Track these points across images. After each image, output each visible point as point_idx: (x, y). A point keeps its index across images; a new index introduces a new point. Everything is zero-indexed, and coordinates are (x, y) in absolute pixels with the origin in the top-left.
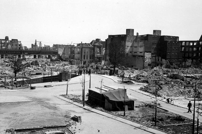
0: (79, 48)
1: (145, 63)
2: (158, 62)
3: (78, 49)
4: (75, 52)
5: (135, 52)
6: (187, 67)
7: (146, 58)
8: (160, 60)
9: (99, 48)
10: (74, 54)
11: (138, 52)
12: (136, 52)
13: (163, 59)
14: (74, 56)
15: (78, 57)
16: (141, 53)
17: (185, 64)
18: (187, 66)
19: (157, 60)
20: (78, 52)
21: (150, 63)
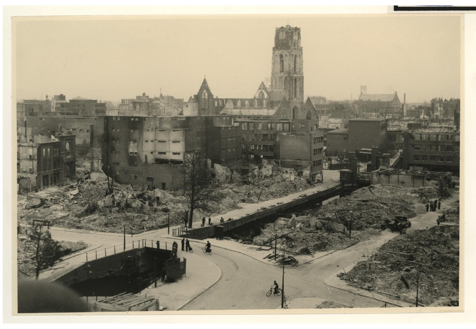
0: (32, 147)
6: (263, 178)
9: (70, 141)
12: (165, 153)
13: (215, 164)
15: (31, 168)
16: (159, 155)
17: (260, 173)
18: (263, 176)
20: (30, 156)
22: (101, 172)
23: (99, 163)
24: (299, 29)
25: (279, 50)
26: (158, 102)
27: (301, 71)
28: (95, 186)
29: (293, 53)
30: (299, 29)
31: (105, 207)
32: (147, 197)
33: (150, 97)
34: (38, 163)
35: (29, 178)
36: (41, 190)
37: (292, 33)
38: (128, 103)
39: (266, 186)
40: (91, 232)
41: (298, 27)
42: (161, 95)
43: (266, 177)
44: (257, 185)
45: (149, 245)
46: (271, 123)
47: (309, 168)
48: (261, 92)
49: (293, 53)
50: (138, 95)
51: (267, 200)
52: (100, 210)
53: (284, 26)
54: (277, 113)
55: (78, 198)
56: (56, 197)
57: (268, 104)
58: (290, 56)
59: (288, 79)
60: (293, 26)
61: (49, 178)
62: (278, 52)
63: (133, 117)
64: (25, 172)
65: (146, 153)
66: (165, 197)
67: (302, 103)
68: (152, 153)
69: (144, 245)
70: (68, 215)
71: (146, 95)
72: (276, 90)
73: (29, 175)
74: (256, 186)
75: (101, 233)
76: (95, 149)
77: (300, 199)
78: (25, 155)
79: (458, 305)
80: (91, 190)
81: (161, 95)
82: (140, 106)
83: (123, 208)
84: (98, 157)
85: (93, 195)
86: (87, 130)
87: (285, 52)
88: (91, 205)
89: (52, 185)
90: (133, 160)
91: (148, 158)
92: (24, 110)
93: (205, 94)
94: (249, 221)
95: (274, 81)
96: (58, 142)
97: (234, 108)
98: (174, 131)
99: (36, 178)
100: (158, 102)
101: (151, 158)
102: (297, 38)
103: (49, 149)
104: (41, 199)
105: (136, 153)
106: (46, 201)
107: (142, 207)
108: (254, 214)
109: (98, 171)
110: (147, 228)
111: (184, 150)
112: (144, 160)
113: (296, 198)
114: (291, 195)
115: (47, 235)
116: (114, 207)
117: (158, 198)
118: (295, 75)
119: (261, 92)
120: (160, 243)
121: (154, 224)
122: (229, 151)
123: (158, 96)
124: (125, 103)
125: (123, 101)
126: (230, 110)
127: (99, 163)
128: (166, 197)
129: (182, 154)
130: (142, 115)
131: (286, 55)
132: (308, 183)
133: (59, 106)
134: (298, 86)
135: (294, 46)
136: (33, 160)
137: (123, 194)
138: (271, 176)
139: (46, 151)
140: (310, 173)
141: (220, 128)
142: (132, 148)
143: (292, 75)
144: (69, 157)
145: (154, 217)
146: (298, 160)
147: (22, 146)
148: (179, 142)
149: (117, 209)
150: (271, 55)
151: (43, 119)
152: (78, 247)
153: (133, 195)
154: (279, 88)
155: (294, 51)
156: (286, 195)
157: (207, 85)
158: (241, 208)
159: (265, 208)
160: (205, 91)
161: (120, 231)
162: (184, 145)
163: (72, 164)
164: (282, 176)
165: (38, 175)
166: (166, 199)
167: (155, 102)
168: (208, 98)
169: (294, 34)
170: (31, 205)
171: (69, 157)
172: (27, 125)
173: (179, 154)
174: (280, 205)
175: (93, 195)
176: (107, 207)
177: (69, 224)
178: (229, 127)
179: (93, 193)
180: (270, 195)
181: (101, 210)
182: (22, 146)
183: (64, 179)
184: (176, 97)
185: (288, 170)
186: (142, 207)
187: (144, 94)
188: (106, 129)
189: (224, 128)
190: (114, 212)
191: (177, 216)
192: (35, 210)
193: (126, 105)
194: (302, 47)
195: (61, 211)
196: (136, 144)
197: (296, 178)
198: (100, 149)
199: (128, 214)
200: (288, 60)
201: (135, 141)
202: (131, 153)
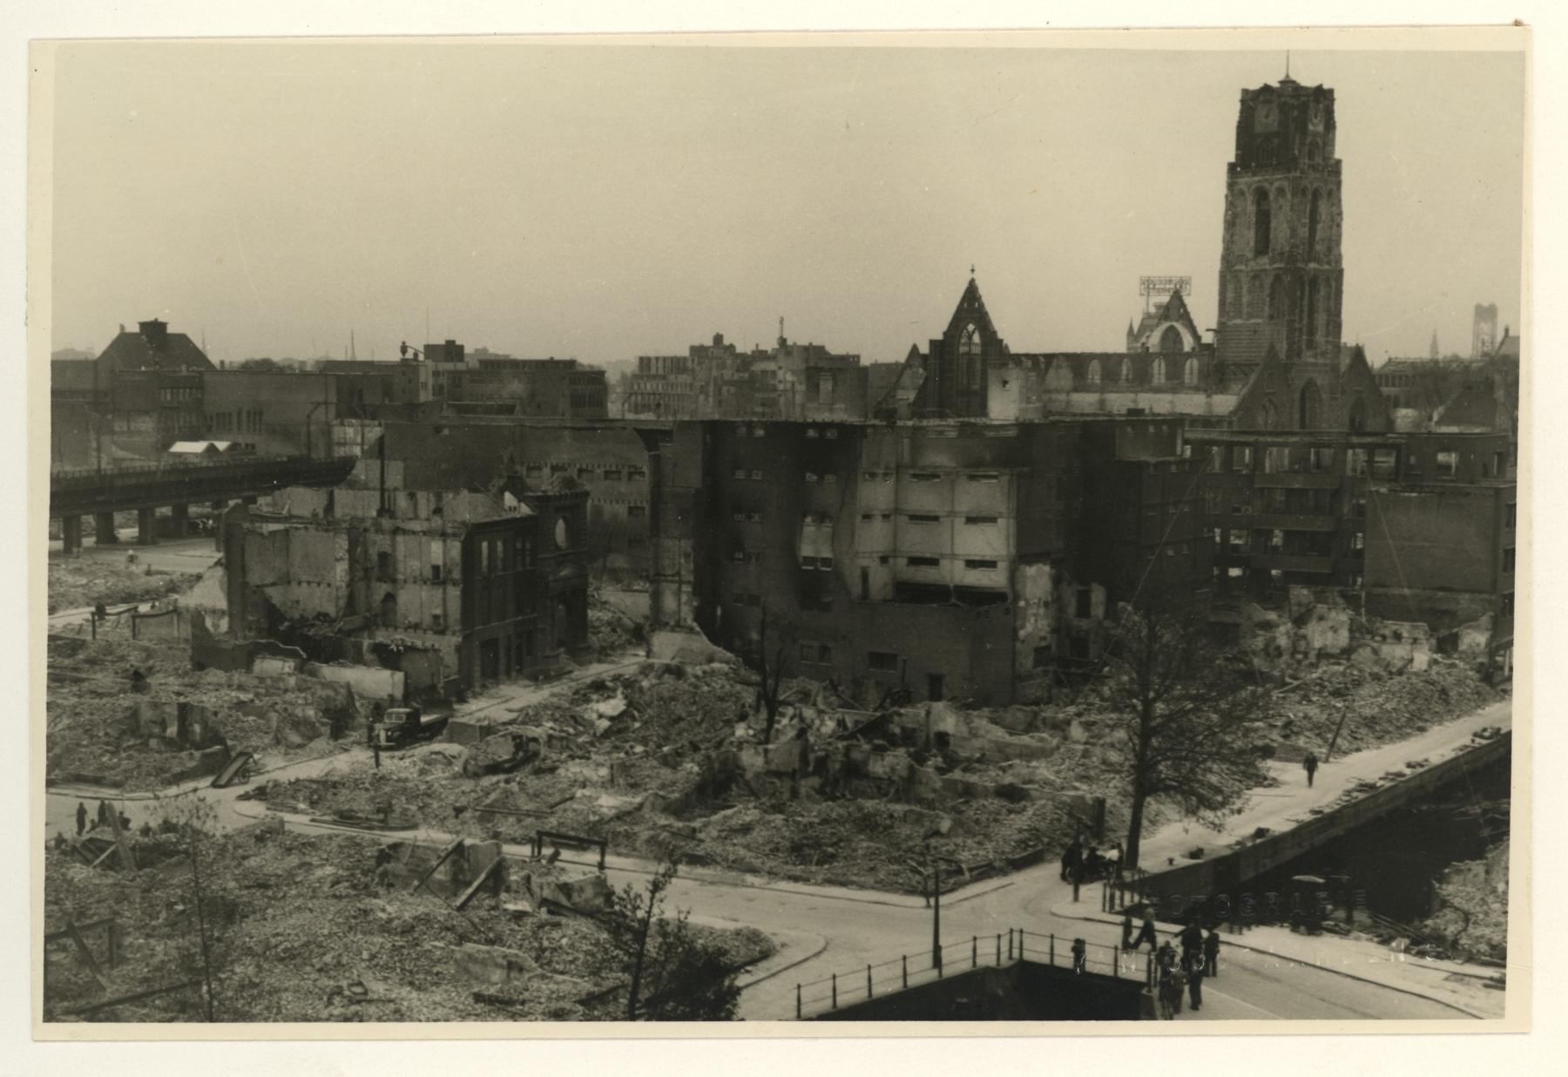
0: (443, 535)
1: (1018, 645)
2: (1084, 624)
3: (436, 547)
4: (401, 566)
5: (915, 561)
6: (1312, 659)
7: (1025, 609)
8: (1098, 611)
10: (394, 581)
11: (953, 556)
12: (933, 562)
14: (390, 598)
15: (438, 612)
16: (912, 569)
17: (1297, 638)
18: (1313, 654)
19: (1072, 609)
20: (436, 568)
21: (1043, 644)
22: (691, 630)
23: (684, 598)
24: (1331, 91)
25: (1254, 174)
26: (772, 366)
27: (1335, 252)
28: (683, 685)
29: (1305, 182)
30: (1331, 91)
31: (769, 773)
32: (897, 730)
33: (739, 350)
34: (466, 596)
35: (436, 651)
36: (475, 696)
37: (1304, 108)
38: (661, 372)
39: (1337, 693)
40: (749, 878)
41: (1326, 87)
42: (783, 341)
43: (1323, 655)
44: (1298, 687)
45: (1036, 952)
46: (1319, 446)
47: (1485, 620)
48: (1172, 328)
49: (1305, 182)
50: (697, 343)
51: (1358, 750)
52: (747, 783)
53: (1275, 84)
54: (1244, 407)
55: (626, 729)
56: (550, 724)
57: (1204, 374)
58: (1294, 195)
59: (1287, 279)
60: (1307, 80)
61: (502, 652)
62: (1247, 181)
63: (815, 425)
64: (416, 627)
65: (865, 562)
66: (973, 734)
67: (1335, 368)
68: (884, 560)
69: (1016, 953)
70: (640, 807)
71: (726, 342)
72: (1238, 321)
73: (430, 640)
74: (1294, 690)
75: (791, 886)
76: (668, 543)
77: (1482, 747)
78: (415, 564)
79: (1502, 1016)
80: (673, 699)
81: (783, 341)
82: (835, 384)
83: (837, 781)
84: (678, 574)
85: (680, 719)
86: (607, 473)
87: (1276, 181)
88: (716, 765)
89: (508, 674)
90: (814, 585)
91: (871, 581)
92: (333, 398)
93: (970, 337)
94: (1320, 839)
95: (1230, 287)
96: (529, 518)
97: (1076, 390)
98: (972, 477)
99: (459, 649)
100: (772, 366)
101: (880, 578)
102: (1321, 128)
103: (499, 544)
104: (514, 738)
105: (826, 561)
106: (532, 746)
107: (912, 778)
108: (1339, 811)
109: (679, 626)
110: (971, 870)
111: (1013, 550)
112: (857, 590)
113: (1467, 740)
114: (1436, 728)
115: (596, 895)
116: (806, 775)
117: (942, 738)
118: (1312, 265)
119: (1172, 328)
120: (1088, 948)
121: (988, 852)
122: (1170, 553)
123: (770, 345)
124: (653, 372)
125: (644, 362)
126: (1063, 397)
127: (684, 598)
128: (976, 736)
129: (1002, 566)
130: (841, 415)
131: (1281, 191)
132: (1482, 680)
133: (443, 380)
134: (1321, 306)
135: (1311, 155)
136: (444, 583)
137: (802, 719)
138: (1347, 652)
139: (492, 549)
140: (1488, 644)
141: (1141, 466)
142: (813, 543)
143: (1299, 265)
144: (565, 572)
145: (977, 822)
146: (1442, 589)
147: (405, 532)
148: (993, 520)
149: (815, 781)
150: (1223, 190)
151: (446, 432)
152: (743, 951)
153: (841, 723)
154: (1250, 316)
155: (1312, 175)
156: (1422, 730)
157: (982, 306)
158: (1274, 783)
159: (1372, 787)
160: (971, 327)
161: (871, 880)
162: (1013, 530)
163: (577, 599)
164: (1375, 652)
165: (465, 638)
166: (977, 743)
167: (758, 367)
168: (984, 353)
169: (1311, 113)
170: (483, 761)
171: (565, 572)
172: (387, 452)
173: (991, 564)
174: (1421, 770)
175: (680, 719)
176: (778, 774)
177: (652, 841)
178: (1170, 463)
179: (679, 709)
180: (1363, 731)
181: (753, 784)
182: (405, 532)
183: (548, 653)
184: (835, 349)
185: (1405, 629)
186: (912, 778)
187: (718, 339)
188: (711, 469)
189: (1156, 465)
190: (808, 797)
191: (1065, 819)
192: (507, 781)
193: (654, 377)
194: (1339, 162)
195: (603, 785)
196: (827, 528)
197: (1436, 662)
198: (686, 545)
199: (870, 805)
200: (1287, 208)
201: (822, 517)
202: (810, 560)
